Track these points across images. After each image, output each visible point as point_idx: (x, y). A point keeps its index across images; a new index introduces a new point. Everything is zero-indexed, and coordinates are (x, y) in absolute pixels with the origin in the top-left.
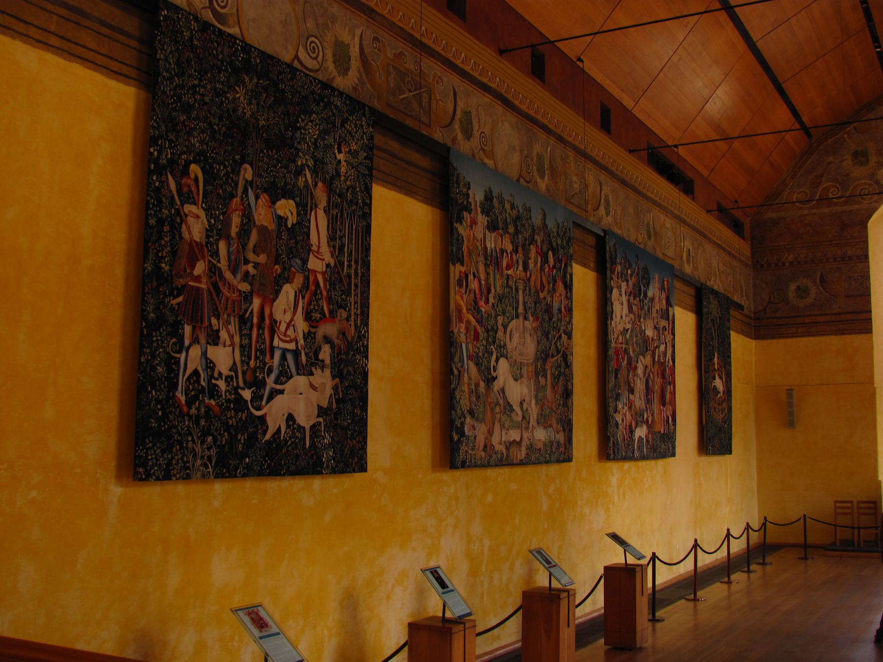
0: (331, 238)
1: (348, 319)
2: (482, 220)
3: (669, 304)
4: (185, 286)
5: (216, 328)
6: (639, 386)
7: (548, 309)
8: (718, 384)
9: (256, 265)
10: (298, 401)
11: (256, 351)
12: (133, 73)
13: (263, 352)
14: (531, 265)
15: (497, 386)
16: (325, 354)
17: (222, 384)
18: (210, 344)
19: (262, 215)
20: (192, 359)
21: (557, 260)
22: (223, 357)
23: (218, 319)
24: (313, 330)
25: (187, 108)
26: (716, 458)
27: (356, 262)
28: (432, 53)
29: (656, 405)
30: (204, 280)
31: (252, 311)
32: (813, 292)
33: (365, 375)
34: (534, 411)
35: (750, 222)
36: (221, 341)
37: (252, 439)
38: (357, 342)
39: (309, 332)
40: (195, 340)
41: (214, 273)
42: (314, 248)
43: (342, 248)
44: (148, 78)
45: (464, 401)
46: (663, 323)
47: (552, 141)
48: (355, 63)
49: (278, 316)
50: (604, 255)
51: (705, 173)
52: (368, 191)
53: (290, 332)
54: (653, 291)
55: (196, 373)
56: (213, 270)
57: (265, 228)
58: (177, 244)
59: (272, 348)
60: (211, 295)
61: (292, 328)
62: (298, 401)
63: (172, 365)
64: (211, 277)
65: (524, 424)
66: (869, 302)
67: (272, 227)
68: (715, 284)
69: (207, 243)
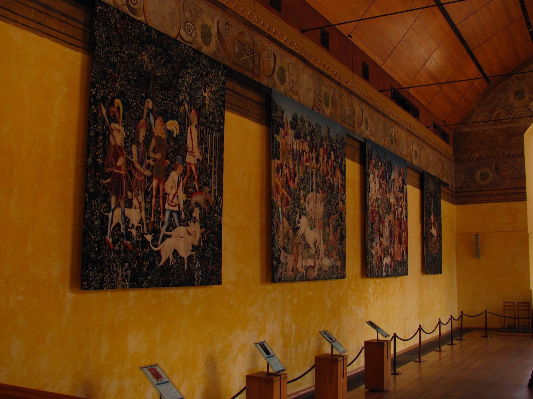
0: (200, 144)
1: (210, 193)
2: (291, 132)
3: (404, 183)
4: (111, 172)
5: (130, 198)
6: (386, 232)
7: (331, 186)
8: (434, 231)
9: (155, 160)
10: (180, 242)
11: (155, 211)
12: (80, 44)
13: (159, 212)
14: (321, 160)
15: (300, 232)
16: (196, 213)
17: (134, 232)
18: (127, 207)
19: (158, 129)
20: (116, 216)
21: (337, 157)
22: (135, 215)
23: (132, 192)
24: (189, 199)
25: (113, 65)
26: (432, 276)
27: (215, 158)
28: (261, 32)
29: (396, 244)
30: (123, 169)
31: (152, 188)
32: (491, 176)
33: (220, 226)
34: (322, 248)
35: (453, 134)
36: (134, 205)
37: (152, 264)
38: (215, 206)
39: (187, 200)
40: (118, 205)
41: (129, 165)
42: (190, 149)
43: (206, 149)
44: (89, 47)
45: (280, 242)
46: (400, 195)
47: (333, 85)
48: (214, 38)
49: (168, 190)
50: (364, 154)
51: (426, 105)
52: (222, 115)
53: (175, 200)
54: (394, 175)
55: (118, 225)
56: (129, 163)
57: (160, 137)
58: (107, 147)
59: (164, 210)
60: (128, 178)
61: (176, 198)
62: (180, 242)
63: (104, 220)
64: (128, 167)
65: (316, 255)
66: (525, 182)
67: (164, 137)
68: (432, 171)
69: (125, 146)
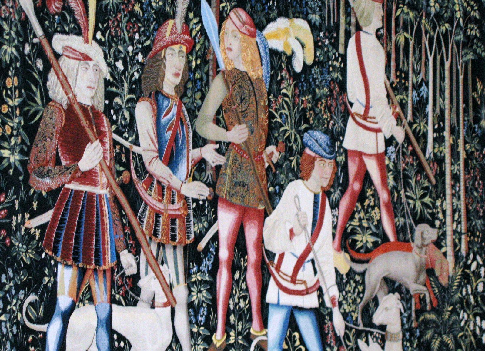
0: (397, 87)
1: (438, 244)
4: (54, 193)
5: (130, 271)
9: (223, 148)
11: (228, 313)
13: (244, 316)
18: (119, 303)
23: (137, 254)
24: (359, 268)
27: (454, 131)
30: (103, 179)
31: (216, 238)
36: (145, 295)
38: (460, 286)
39: (351, 273)
40: (83, 295)
41: (127, 166)
42: (357, 109)
43: (420, 106)
49: (275, 242)
53: (306, 274)
56: (123, 159)
57: (244, 76)
58: (36, 112)
59: (264, 308)
60: (120, 208)
61: (308, 266)
64: (119, 173)
67: (260, 72)
69: (107, 108)
